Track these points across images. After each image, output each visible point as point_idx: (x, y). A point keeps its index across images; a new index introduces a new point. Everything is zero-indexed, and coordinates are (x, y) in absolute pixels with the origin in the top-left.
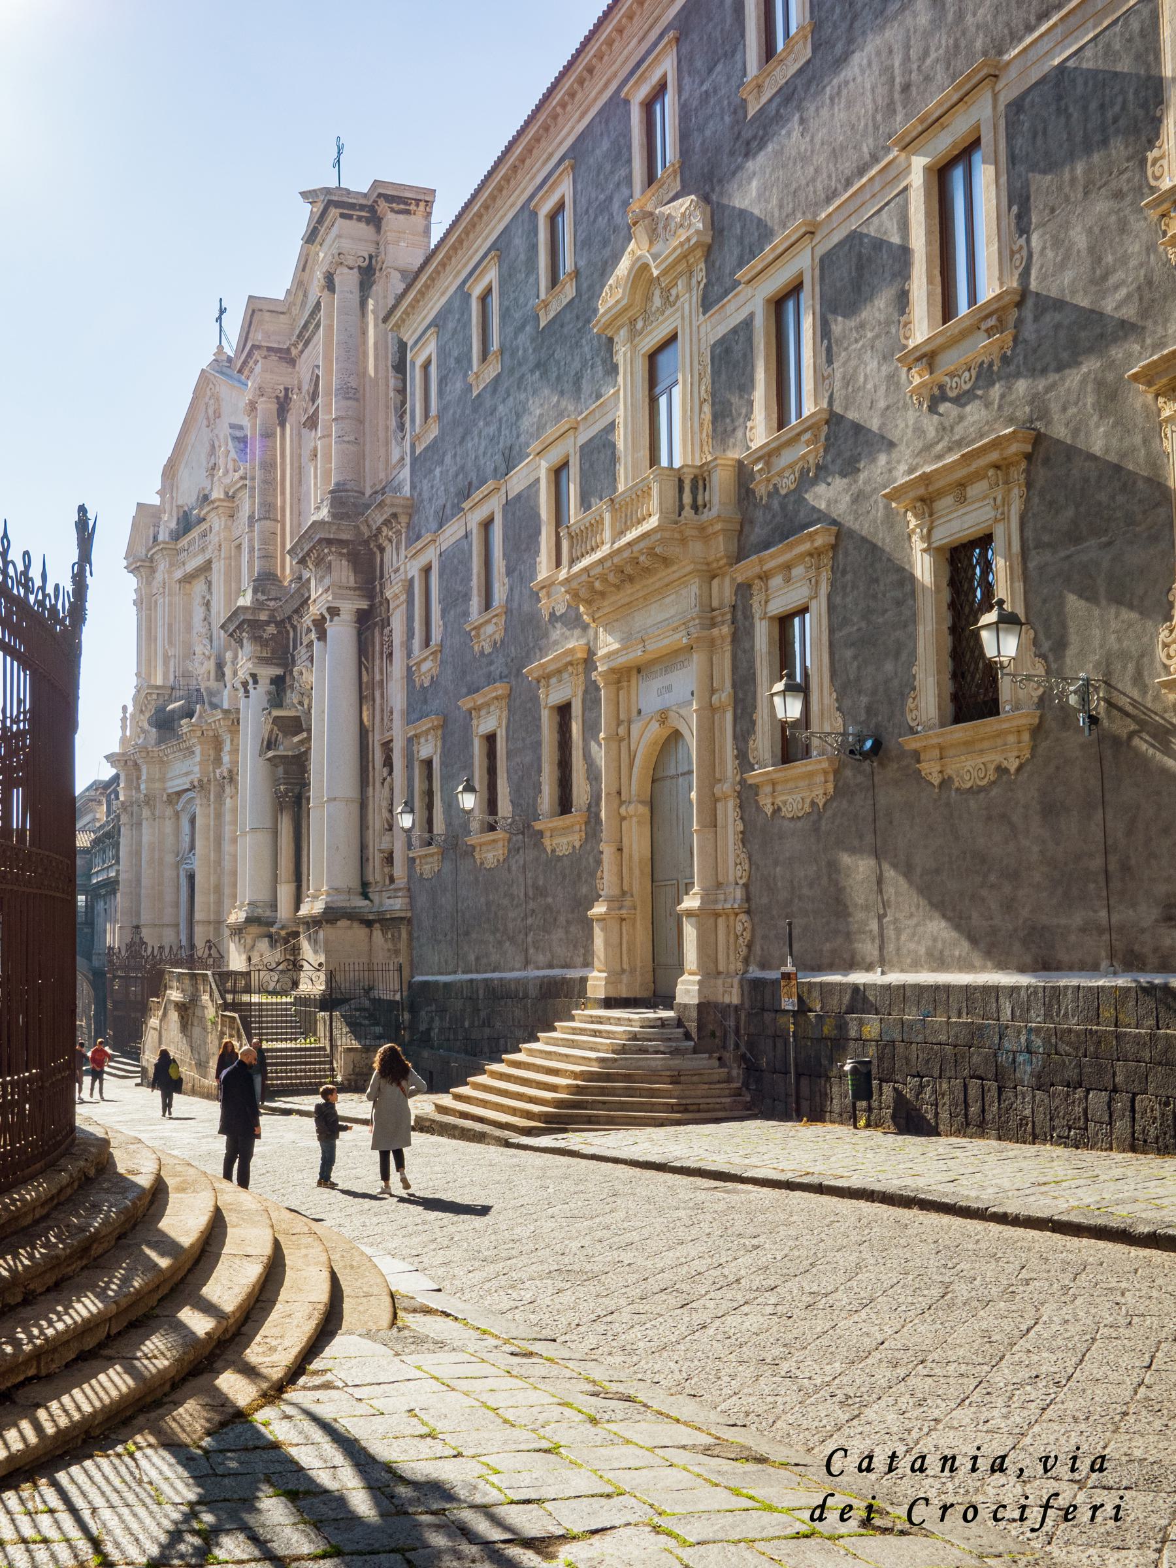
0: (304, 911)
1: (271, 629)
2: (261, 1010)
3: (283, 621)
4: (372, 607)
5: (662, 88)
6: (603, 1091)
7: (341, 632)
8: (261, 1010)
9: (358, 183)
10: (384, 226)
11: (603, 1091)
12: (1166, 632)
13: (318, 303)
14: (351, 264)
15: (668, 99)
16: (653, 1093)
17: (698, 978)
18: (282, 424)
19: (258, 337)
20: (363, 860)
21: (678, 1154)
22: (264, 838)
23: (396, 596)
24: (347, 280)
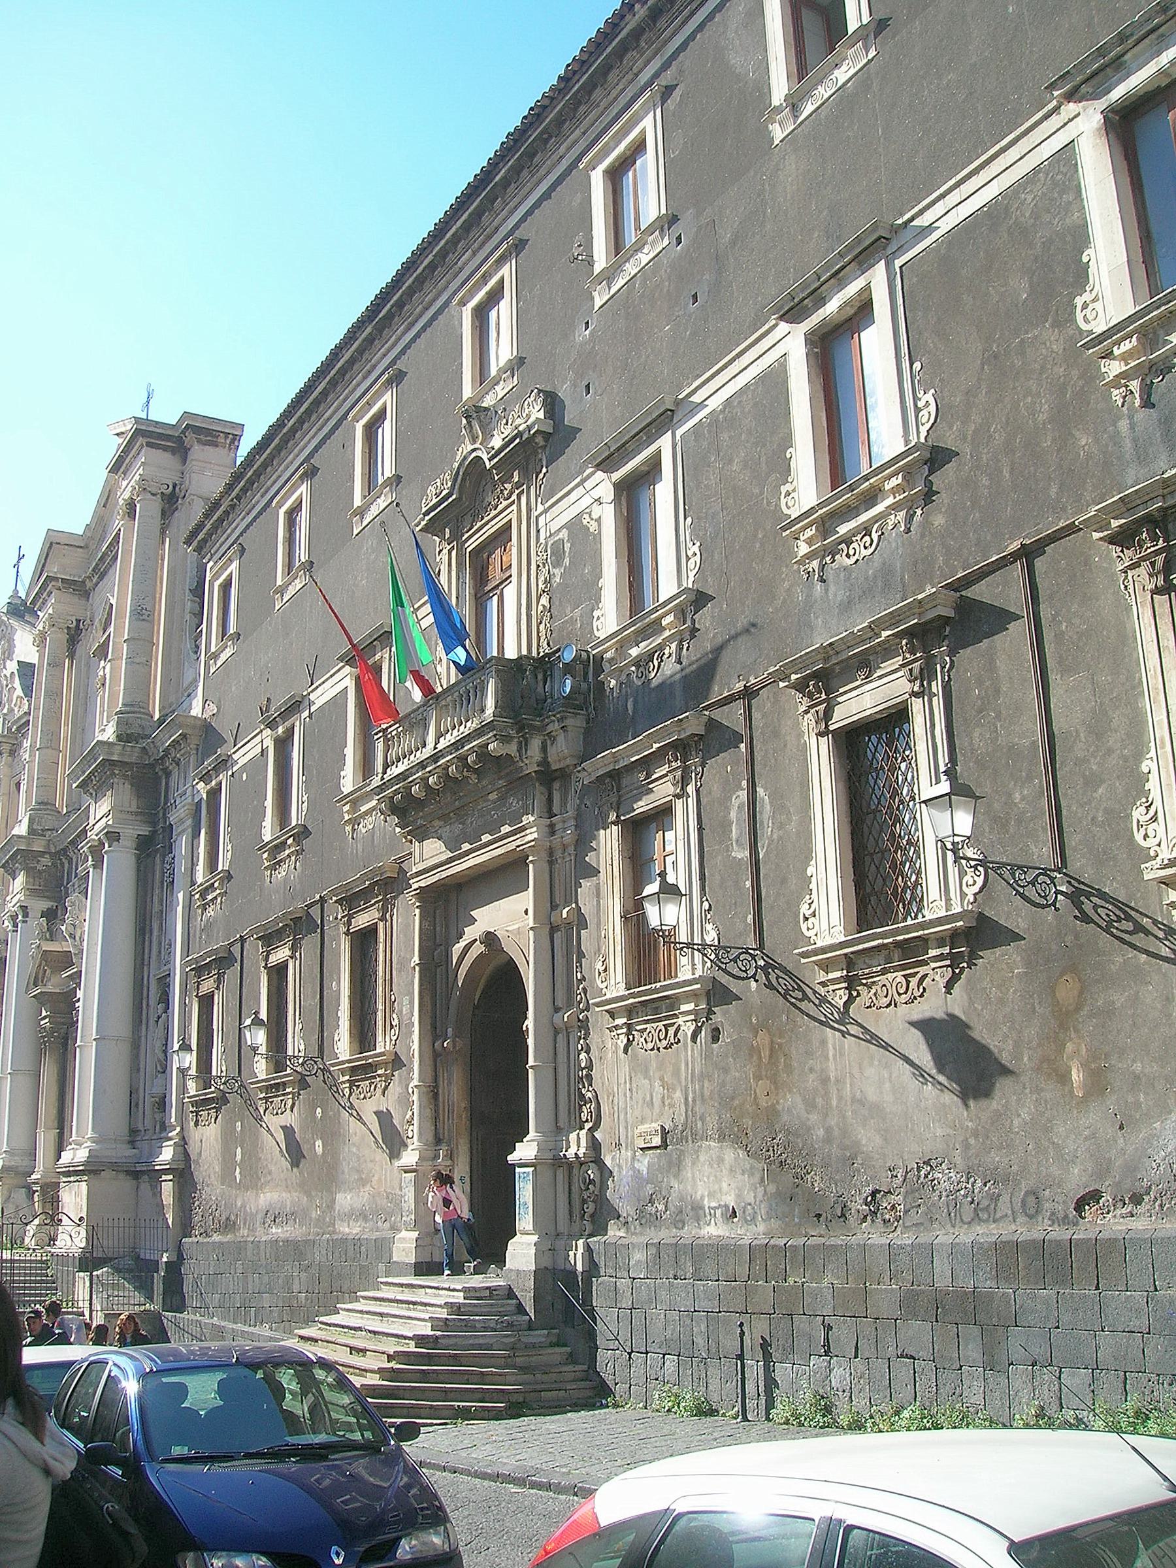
0: (66, 1157)
1: (46, 861)
2: (13, 1268)
3: (58, 852)
4: (154, 832)
5: (381, 416)
6: (424, 1376)
7: (120, 861)
8: (13, 1268)
9: (167, 413)
10: (191, 455)
11: (424, 1376)
12: (1142, 810)
13: (118, 535)
14: (154, 491)
15: (387, 423)
16: (483, 1378)
17: (535, 1238)
18: (72, 656)
19: (53, 569)
20: (133, 1105)
21: (535, 1463)
22: (25, 1082)
23: (182, 821)
24: (148, 509)
